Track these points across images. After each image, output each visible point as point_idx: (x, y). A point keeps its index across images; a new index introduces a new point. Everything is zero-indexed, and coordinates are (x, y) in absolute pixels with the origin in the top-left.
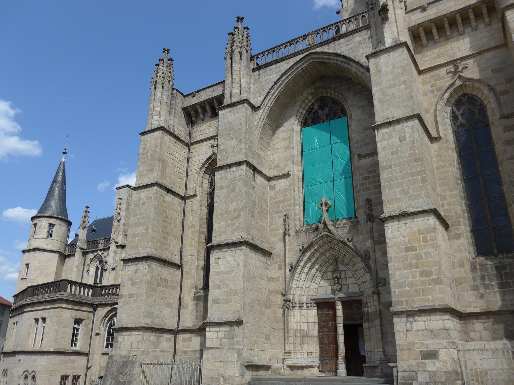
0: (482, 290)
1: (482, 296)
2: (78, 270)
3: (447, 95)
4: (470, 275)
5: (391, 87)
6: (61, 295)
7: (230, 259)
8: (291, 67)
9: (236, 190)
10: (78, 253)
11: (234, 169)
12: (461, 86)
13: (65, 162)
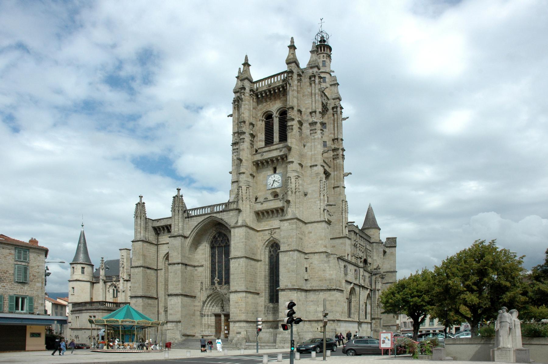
0: (266, 315)
2: (103, 291)
3: (267, 243)
4: (264, 310)
5: (238, 243)
7: (176, 300)
8: (203, 221)
10: (101, 282)
11: (176, 265)
12: (272, 240)
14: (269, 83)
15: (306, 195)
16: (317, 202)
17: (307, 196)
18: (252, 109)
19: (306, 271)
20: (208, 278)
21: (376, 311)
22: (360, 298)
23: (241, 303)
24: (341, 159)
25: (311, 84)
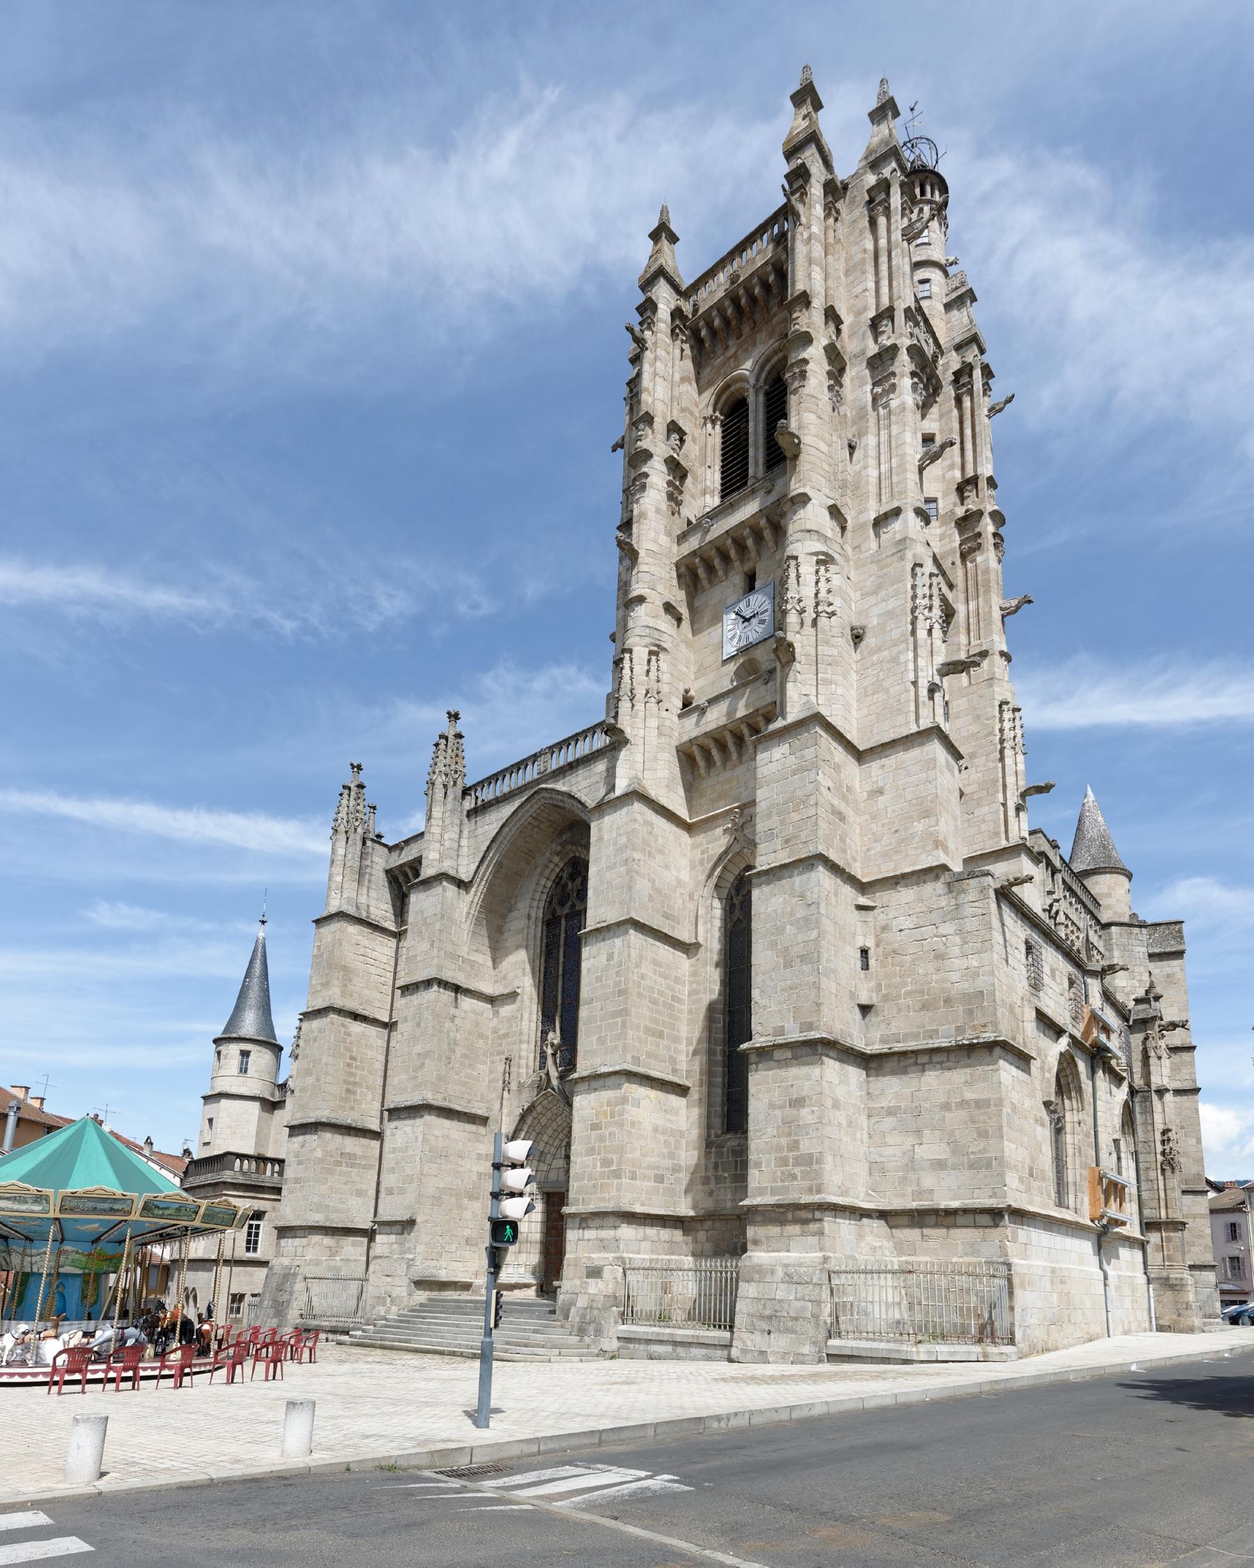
0: (712, 1185)
1: (711, 1194)
5: (609, 868)
6: (227, 1176)
9: (422, 1025)
13: (264, 939)
16: (902, 659)
17: (863, 644)
19: (866, 967)
21: (1161, 1186)
22: (1099, 1114)
23: (611, 1129)
24: (992, 548)
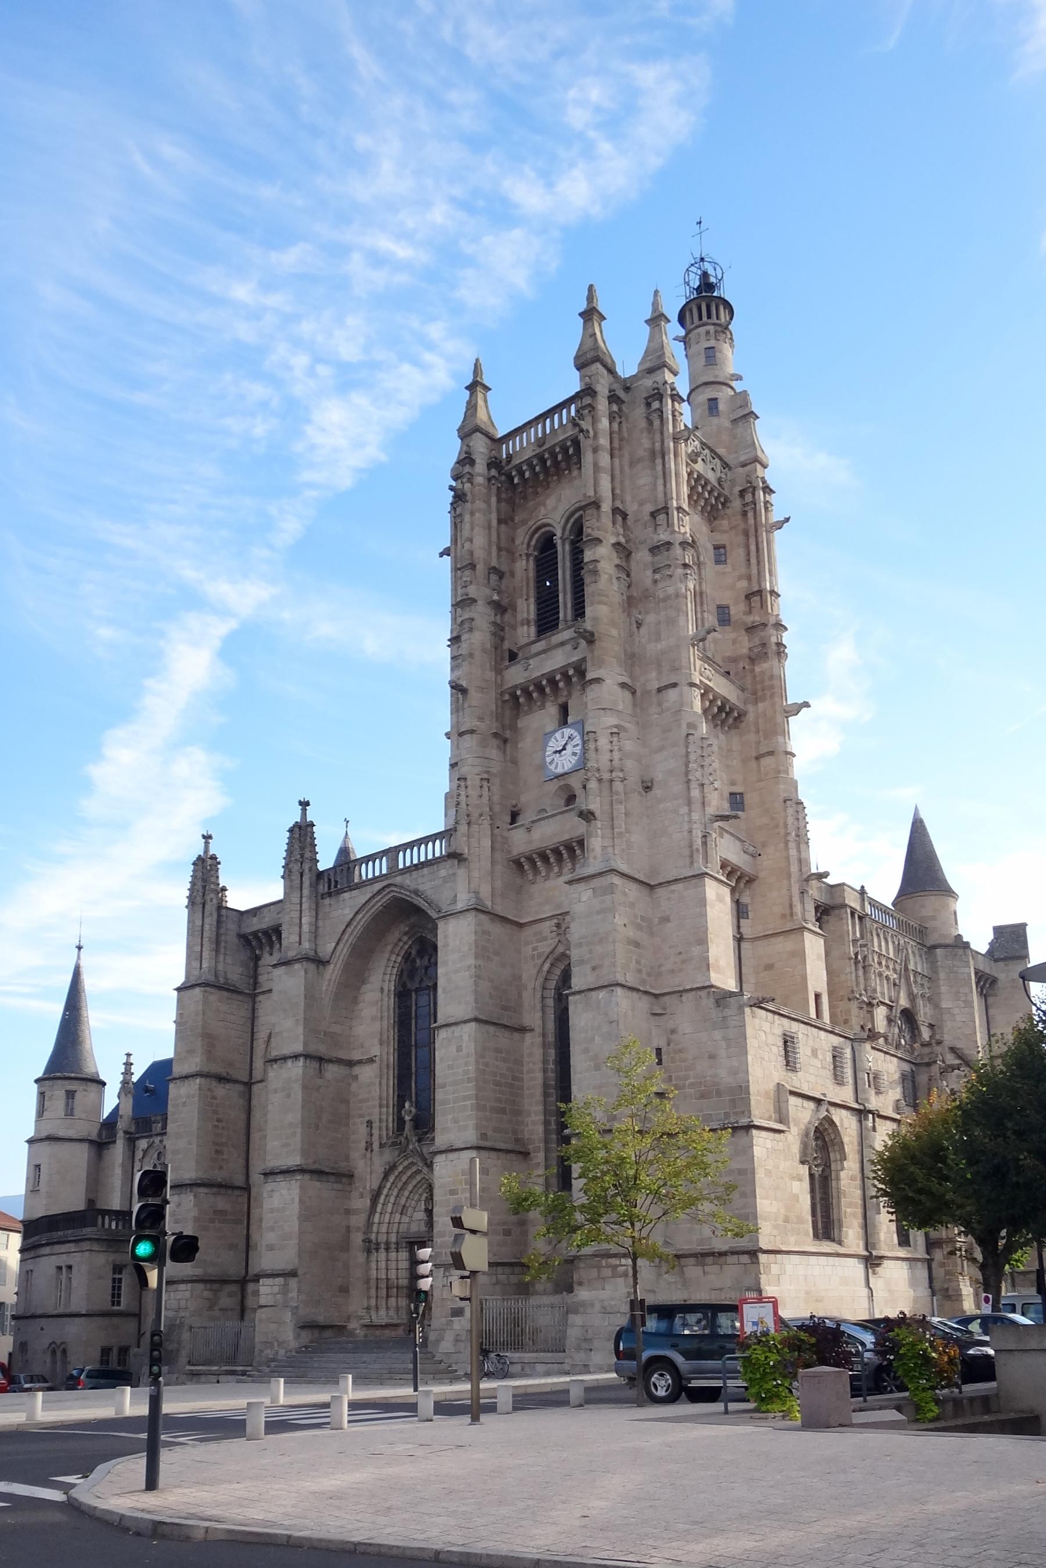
1: (550, 1243)
14: (540, 436)
15: (648, 788)
18: (494, 523)
20: (388, 1107)
25: (650, 422)
